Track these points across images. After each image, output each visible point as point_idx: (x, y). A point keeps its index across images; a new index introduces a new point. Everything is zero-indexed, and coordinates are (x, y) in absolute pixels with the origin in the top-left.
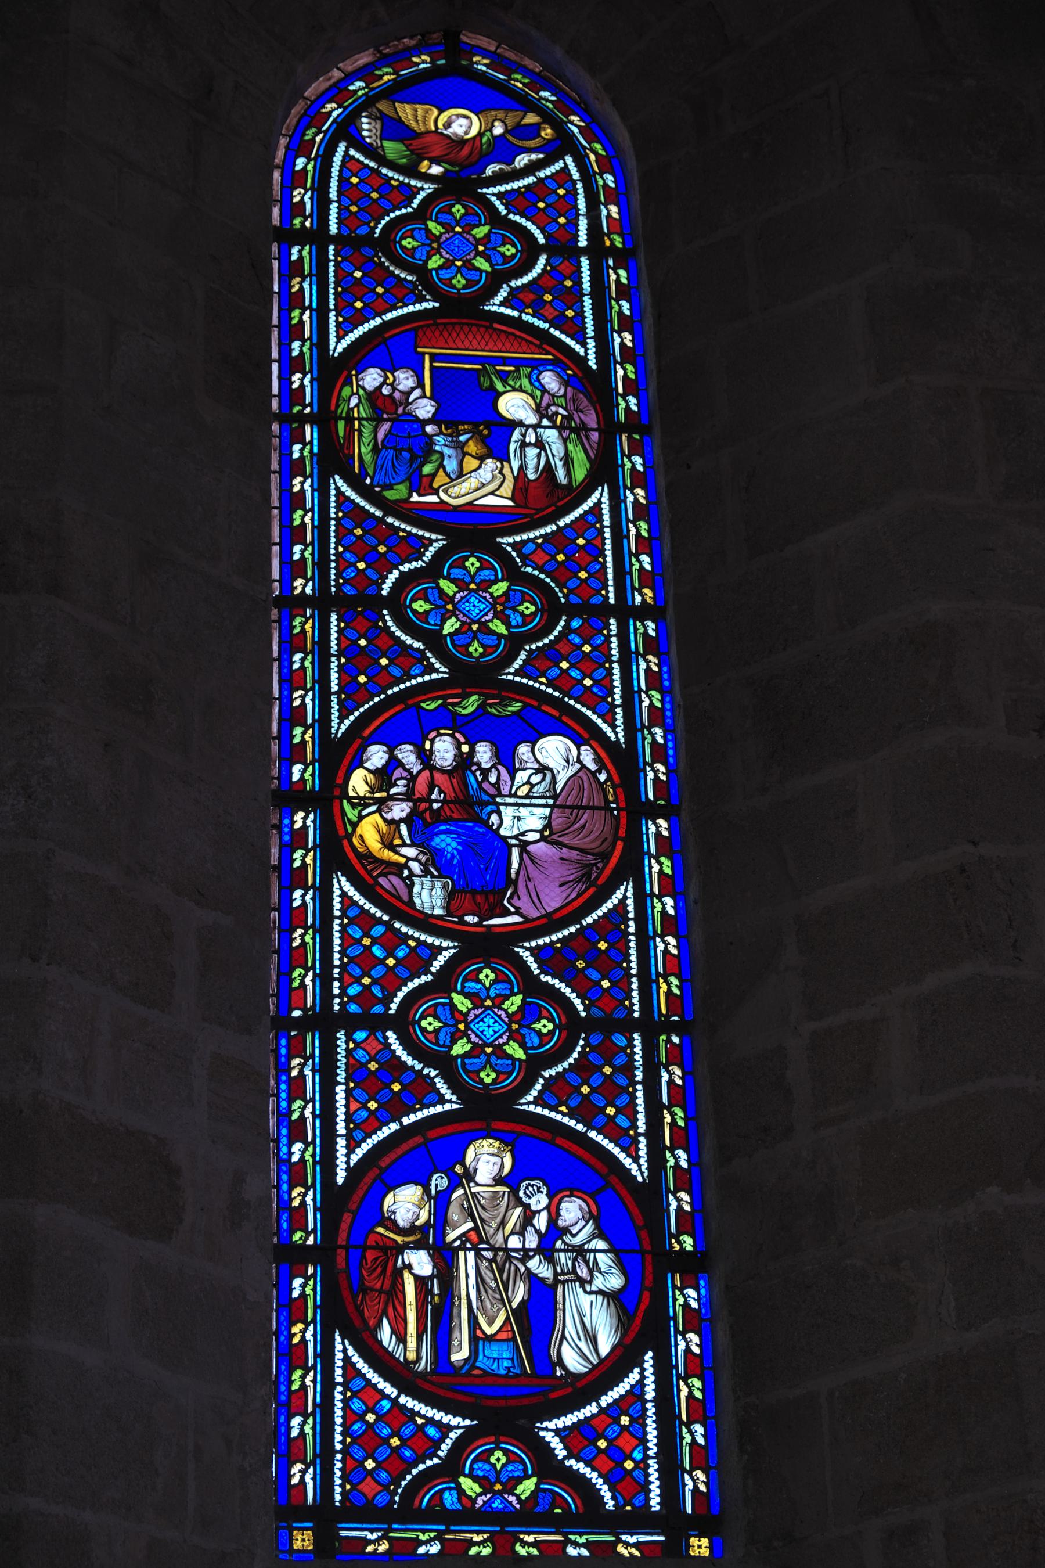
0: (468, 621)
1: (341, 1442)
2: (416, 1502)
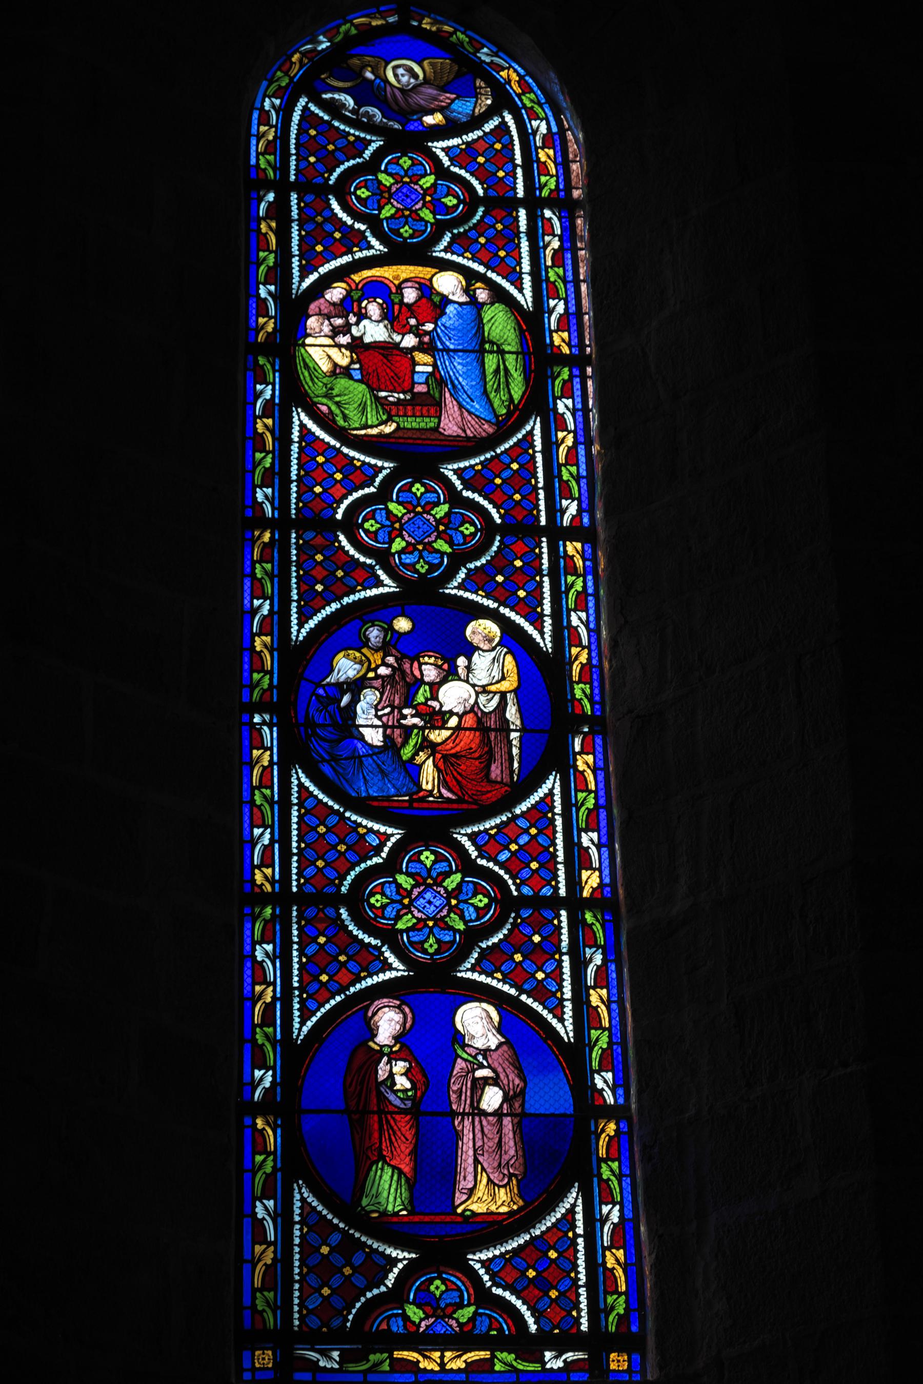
0: (424, 917)
1: (297, 848)
2: (367, 1328)
